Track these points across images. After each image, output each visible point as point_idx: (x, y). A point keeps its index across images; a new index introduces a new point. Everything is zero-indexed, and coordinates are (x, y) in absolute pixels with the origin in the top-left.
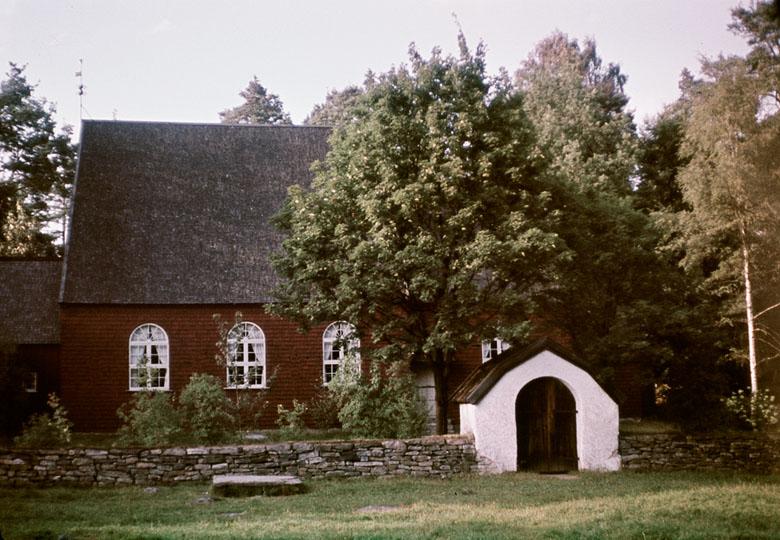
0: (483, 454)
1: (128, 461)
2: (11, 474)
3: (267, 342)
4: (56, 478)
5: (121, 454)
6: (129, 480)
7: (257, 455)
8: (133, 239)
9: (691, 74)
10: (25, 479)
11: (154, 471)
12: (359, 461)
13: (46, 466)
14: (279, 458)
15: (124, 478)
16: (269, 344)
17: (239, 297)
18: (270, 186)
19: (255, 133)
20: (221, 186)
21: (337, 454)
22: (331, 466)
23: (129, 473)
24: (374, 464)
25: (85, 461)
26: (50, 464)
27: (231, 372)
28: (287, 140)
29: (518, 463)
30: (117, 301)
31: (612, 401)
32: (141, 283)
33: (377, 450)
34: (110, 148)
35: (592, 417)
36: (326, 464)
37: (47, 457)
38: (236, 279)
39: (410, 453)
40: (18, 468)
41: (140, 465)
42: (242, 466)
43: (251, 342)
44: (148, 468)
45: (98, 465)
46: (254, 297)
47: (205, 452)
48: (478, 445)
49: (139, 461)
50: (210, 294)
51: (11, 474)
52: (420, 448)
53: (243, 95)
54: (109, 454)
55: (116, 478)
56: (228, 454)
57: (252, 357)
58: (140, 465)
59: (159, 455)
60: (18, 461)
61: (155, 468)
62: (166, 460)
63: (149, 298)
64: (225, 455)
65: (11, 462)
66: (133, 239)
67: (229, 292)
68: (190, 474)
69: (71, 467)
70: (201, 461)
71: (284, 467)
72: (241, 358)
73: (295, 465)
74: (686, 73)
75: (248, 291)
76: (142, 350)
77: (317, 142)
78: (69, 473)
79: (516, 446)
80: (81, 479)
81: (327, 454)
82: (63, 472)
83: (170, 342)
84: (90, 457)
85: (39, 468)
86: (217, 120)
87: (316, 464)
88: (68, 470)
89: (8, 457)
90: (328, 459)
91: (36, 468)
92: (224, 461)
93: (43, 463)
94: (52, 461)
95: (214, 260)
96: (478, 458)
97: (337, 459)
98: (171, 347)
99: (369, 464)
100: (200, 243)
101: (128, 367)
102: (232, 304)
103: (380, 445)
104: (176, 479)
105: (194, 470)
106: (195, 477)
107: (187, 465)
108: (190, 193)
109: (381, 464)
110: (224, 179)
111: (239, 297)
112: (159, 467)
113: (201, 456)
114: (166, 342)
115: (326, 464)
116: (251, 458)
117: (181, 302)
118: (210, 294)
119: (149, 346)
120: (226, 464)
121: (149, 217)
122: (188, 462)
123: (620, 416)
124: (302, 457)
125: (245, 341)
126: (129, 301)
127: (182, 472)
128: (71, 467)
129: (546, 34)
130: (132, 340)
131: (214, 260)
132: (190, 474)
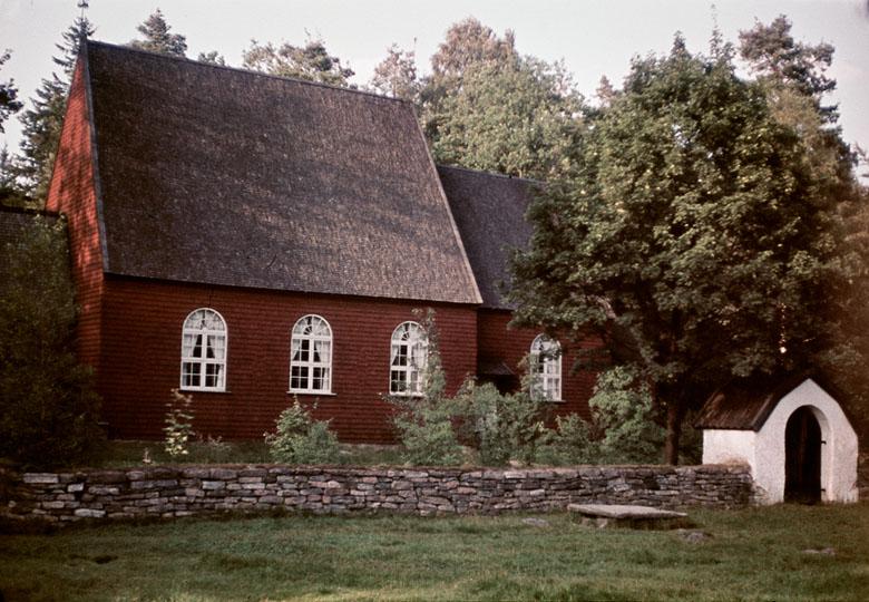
0: (759, 484)
1: (449, 485)
2: (326, 500)
3: (334, 340)
4: (376, 505)
5: (442, 477)
6: (451, 508)
7: (569, 481)
8: (176, 201)
9: (610, 83)
10: (343, 507)
11: (476, 497)
12: (658, 489)
13: (364, 490)
14: (591, 484)
15: (445, 506)
16: (337, 343)
17: (309, 284)
18: (315, 155)
19: (284, 87)
20: (260, 147)
21: (641, 482)
22: (636, 495)
23: (450, 500)
24: (672, 492)
25: (405, 484)
26: (368, 487)
27: (394, 377)
28: (320, 101)
29: (786, 494)
30: (174, 277)
31: (854, 433)
32: (198, 257)
33: (672, 478)
34: (125, 80)
35: (840, 448)
36: (633, 492)
37: (365, 479)
38: (302, 262)
39: (700, 482)
40: (333, 493)
41: (461, 490)
42: (557, 493)
43: (212, 333)
44: (469, 494)
45: (418, 490)
46: (326, 286)
47: (524, 476)
48: (755, 474)
49: (460, 486)
50: (276, 277)
51: (326, 500)
52: (707, 476)
53: (142, 29)
54: (430, 476)
55: (437, 505)
56: (544, 479)
57: (317, 358)
58: (461, 490)
59: (479, 478)
60: (333, 484)
61: (476, 494)
62: (488, 485)
63: (210, 279)
64: (541, 479)
65: (324, 485)
66: (176, 201)
67: (297, 278)
68: (509, 501)
69: (390, 492)
70: (519, 486)
71: (596, 494)
72: (305, 357)
73: (605, 493)
74: (605, 81)
75: (317, 279)
76: (194, 341)
77: (351, 107)
78: (388, 499)
79: (784, 477)
80: (402, 506)
81: (633, 481)
82: (382, 498)
83: (229, 332)
84: (409, 480)
85: (357, 493)
86: (235, 61)
87: (623, 492)
88: (387, 495)
89: (322, 478)
90: (635, 486)
91: (352, 492)
92: (540, 487)
93: (360, 486)
94: (370, 484)
95: (273, 237)
96: (754, 487)
97: (642, 487)
98: (229, 338)
99: (668, 493)
100: (253, 214)
101: (180, 360)
102: (302, 292)
103: (674, 473)
104: (496, 507)
105: (514, 497)
106: (515, 506)
107: (507, 490)
108: (228, 151)
109: (677, 493)
110: (263, 140)
111: (309, 284)
112: (480, 493)
113: (518, 480)
114: (225, 333)
115: (633, 492)
116: (564, 484)
117: (247, 285)
118: (276, 277)
119: (206, 334)
120: (543, 491)
121: (187, 175)
122: (507, 487)
123: (860, 451)
124: (611, 484)
125: (312, 338)
126: (188, 278)
127: (501, 499)
128: (390, 492)
129: (460, 19)
130: (187, 327)
131: (273, 237)
132: (509, 501)
